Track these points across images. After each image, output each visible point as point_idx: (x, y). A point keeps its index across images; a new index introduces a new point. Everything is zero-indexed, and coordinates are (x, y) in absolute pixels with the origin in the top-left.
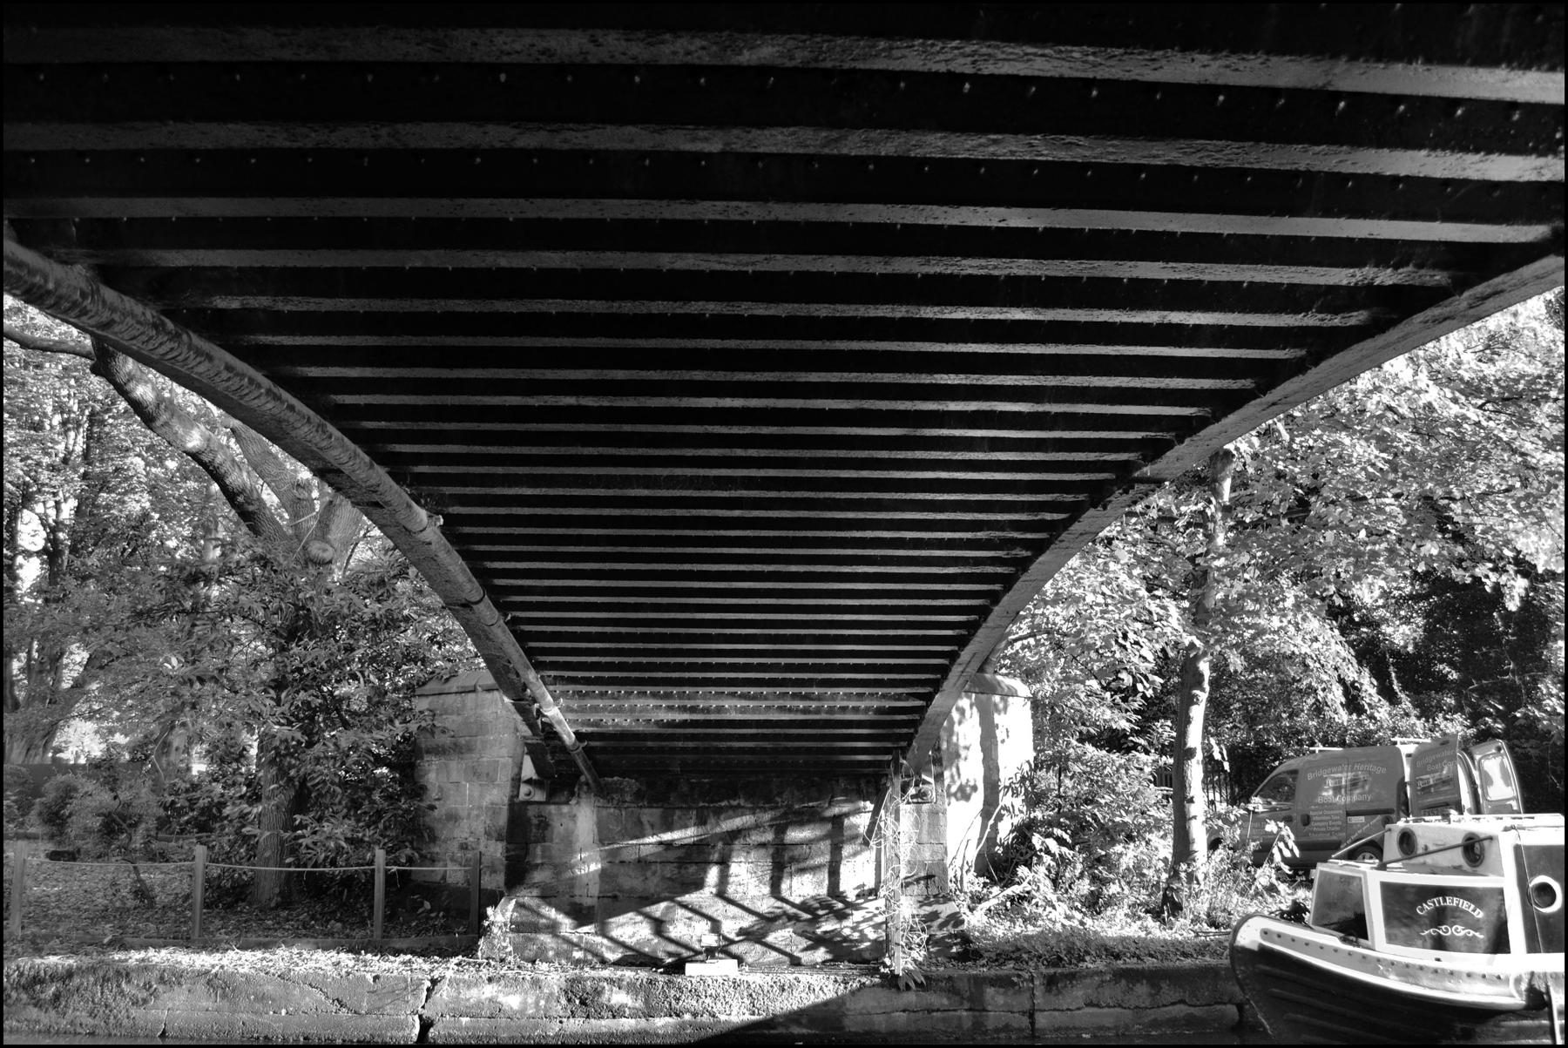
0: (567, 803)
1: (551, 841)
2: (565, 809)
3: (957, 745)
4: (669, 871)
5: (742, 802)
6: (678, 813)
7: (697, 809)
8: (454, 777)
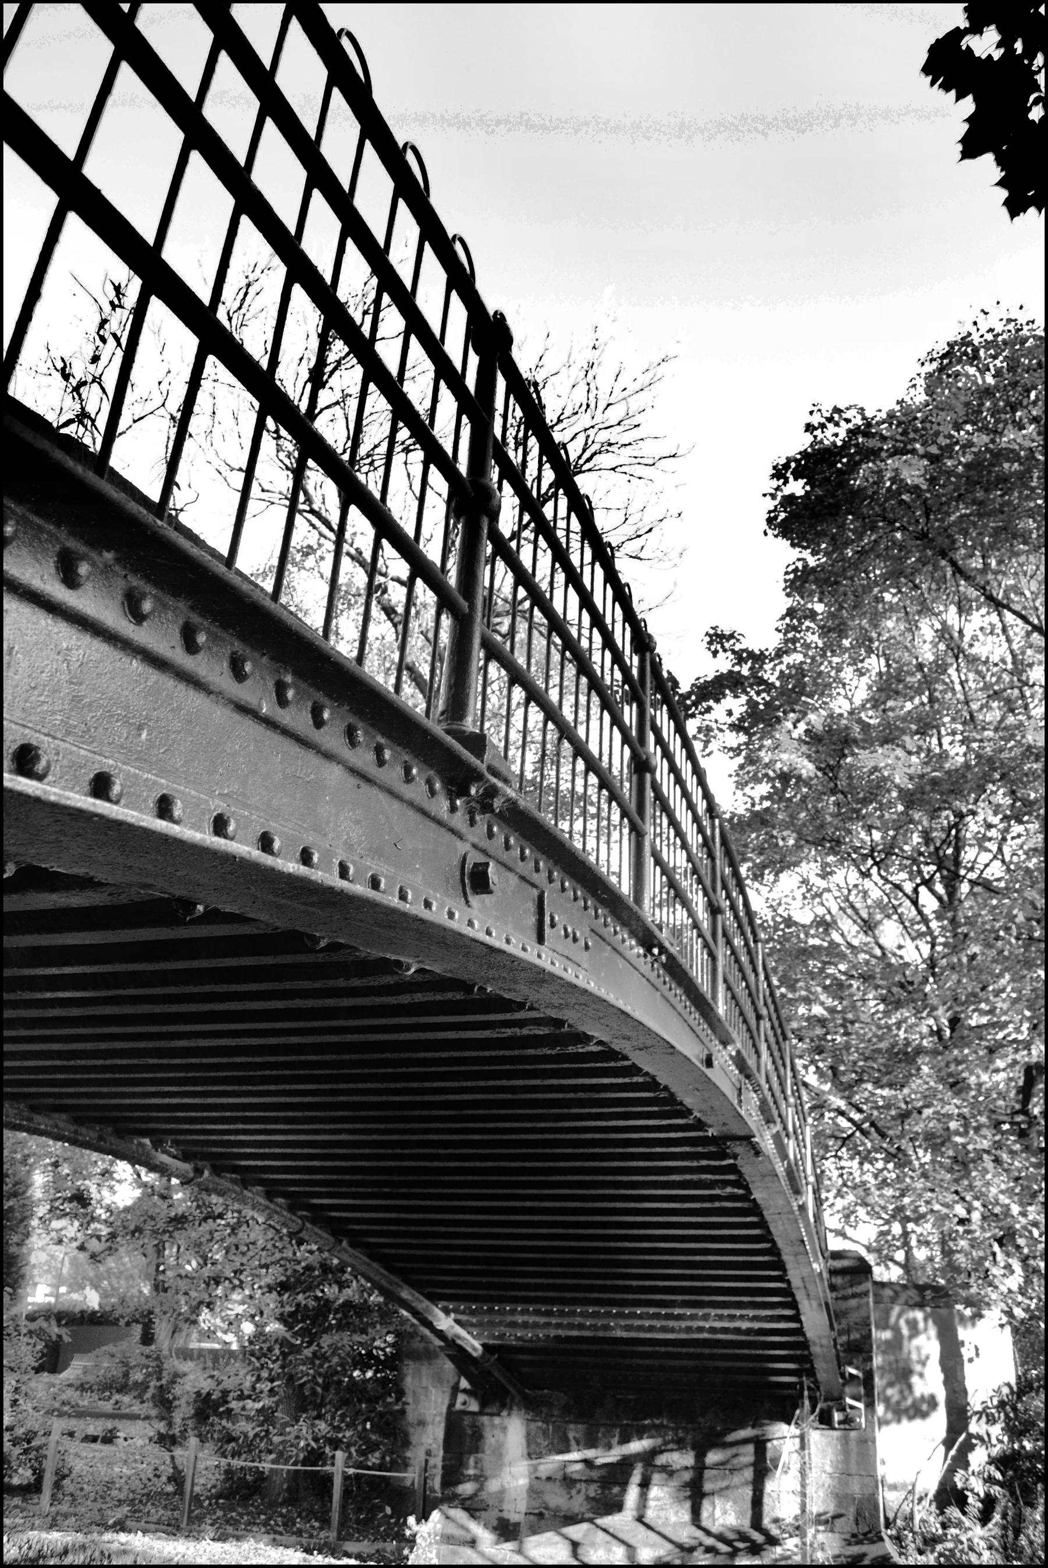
0: (498, 1415)
2: (497, 1420)
3: (908, 1359)
4: (593, 1490)
5: (665, 1422)
6: (602, 1430)
7: (621, 1426)
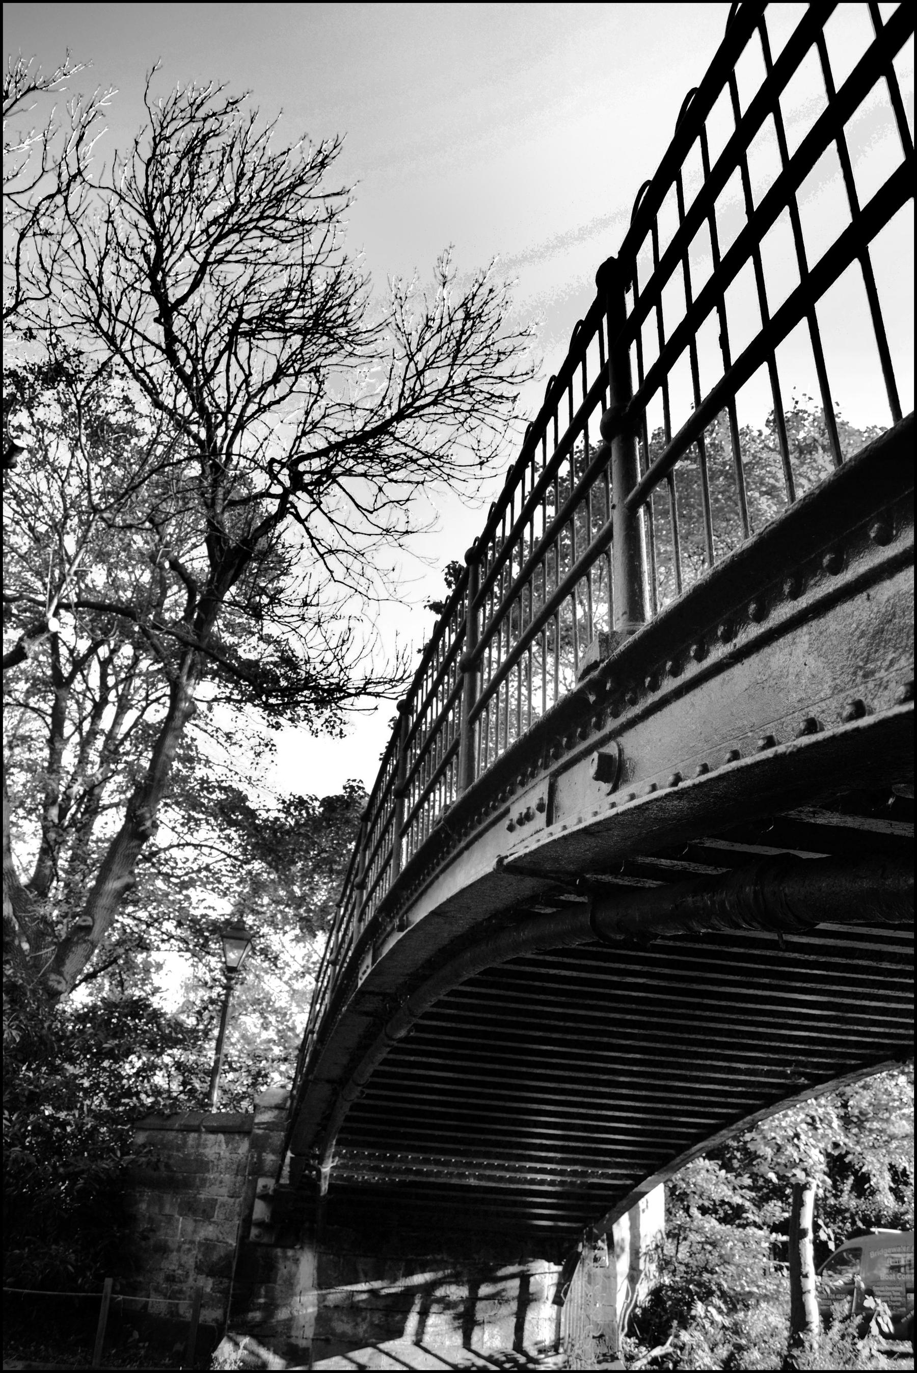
1: (275, 1282)
2: (290, 1253)
8: (167, 1210)
